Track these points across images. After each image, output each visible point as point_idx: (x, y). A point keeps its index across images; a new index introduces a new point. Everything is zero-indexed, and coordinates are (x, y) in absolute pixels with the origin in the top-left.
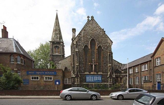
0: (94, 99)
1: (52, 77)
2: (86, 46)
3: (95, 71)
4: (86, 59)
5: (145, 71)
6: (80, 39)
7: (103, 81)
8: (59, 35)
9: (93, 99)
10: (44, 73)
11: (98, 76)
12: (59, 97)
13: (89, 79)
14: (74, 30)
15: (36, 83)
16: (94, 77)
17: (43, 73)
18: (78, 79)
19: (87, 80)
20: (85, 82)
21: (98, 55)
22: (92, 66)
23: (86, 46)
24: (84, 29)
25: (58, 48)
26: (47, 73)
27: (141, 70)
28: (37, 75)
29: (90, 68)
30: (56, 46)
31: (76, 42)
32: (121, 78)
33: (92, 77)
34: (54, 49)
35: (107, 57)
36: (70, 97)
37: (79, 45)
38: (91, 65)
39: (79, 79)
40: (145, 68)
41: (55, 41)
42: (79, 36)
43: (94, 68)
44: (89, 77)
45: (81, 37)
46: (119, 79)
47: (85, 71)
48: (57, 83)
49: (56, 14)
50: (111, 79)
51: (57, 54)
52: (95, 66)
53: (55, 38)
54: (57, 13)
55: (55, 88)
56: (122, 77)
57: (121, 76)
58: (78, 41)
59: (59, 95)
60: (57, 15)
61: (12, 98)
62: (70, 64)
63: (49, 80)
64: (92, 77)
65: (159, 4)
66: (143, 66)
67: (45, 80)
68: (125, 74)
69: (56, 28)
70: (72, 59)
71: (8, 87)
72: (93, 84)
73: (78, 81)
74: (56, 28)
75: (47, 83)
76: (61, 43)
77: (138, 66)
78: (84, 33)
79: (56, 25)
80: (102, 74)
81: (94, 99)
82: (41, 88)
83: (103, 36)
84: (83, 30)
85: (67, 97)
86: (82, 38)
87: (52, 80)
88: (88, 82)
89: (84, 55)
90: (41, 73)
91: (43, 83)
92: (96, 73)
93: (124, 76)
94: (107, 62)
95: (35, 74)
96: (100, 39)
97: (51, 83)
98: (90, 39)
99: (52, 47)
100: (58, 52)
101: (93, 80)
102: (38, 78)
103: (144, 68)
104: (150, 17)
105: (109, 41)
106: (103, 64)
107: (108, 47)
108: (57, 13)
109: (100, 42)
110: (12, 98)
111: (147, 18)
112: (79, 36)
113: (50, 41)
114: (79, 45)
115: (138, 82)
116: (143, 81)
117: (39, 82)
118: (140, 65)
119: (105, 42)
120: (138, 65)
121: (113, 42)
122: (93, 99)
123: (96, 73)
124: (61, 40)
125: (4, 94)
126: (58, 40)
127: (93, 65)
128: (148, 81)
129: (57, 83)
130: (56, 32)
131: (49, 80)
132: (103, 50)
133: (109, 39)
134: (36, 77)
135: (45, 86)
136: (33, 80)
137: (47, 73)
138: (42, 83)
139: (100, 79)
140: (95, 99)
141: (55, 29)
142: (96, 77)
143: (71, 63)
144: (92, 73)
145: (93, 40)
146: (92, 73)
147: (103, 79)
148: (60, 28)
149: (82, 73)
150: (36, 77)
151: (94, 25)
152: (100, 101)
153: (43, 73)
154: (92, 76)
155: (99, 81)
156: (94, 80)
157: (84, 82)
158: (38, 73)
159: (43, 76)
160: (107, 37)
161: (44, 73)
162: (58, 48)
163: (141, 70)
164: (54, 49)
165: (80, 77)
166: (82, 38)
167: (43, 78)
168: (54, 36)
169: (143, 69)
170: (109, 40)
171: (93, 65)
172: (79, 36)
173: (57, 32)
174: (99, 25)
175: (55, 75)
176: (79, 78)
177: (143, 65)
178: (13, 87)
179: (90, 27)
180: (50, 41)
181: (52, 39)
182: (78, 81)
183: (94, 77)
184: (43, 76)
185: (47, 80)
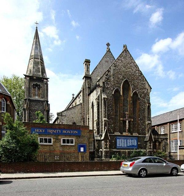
0: (143, 175)
1: (73, 140)
2: (117, 91)
3: (129, 131)
4: (116, 112)
5: (175, 132)
6: (108, 79)
7: (139, 147)
8: (41, 65)
9: (174, 174)
10: (62, 132)
11: (133, 139)
12: (120, 172)
13: (121, 143)
14: (87, 62)
15: (46, 149)
16: (127, 141)
17: (59, 131)
18: (106, 143)
19: (118, 145)
20: (115, 148)
21: (132, 106)
22: (124, 122)
23: (117, 91)
24: (115, 63)
25: (39, 89)
26: (65, 132)
27: (170, 131)
28: (49, 134)
29: (122, 125)
30: (37, 85)
31: (104, 83)
32: (160, 143)
33: (125, 140)
34: (32, 90)
35: (144, 110)
36: (174, 170)
37: (108, 87)
38: (123, 121)
39: (108, 143)
40: (176, 128)
41: (34, 75)
42: (107, 74)
43: (127, 126)
44: (120, 140)
45: (110, 76)
46: (157, 144)
47: (115, 131)
48: (82, 149)
49: (36, 28)
50: (150, 143)
51: (37, 98)
52: (129, 122)
53: (34, 71)
54: (37, 27)
55: (78, 158)
56: (161, 141)
57: (159, 140)
58: (105, 81)
59: (118, 169)
60: (37, 30)
61: (42, 178)
62: (80, 118)
63: (45, 144)
64: (125, 140)
65: (157, 39)
66: (173, 125)
67: (62, 144)
68: (164, 137)
69: (35, 52)
70: (84, 109)
71: (21, 157)
72: (127, 151)
73: (106, 146)
74: (36, 54)
75: (66, 150)
76: (45, 80)
77: (165, 125)
78: (114, 69)
79: (36, 48)
80: (138, 135)
81: (143, 175)
82: (57, 158)
83: (140, 78)
84: (113, 65)
85: (144, 171)
86: (112, 78)
87: (74, 144)
88: (120, 148)
89: (114, 104)
90: (57, 131)
91: (58, 149)
92: (130, 135)
93: (164, 139)
94: (144, 117)
95: (46, 134)
96: (136, 82)
97: (72, 150)
98: (123, 80)
99: (29, 85)
100: (39, 95)
101: (125, 146)
102: (50, 142)
103: (175, 128)
104: (147, 54)
105: (147, 86)
106: (139, 120)
107: (145, 95)
108: (37, 27)
109: (135, 87)
110: (42, 178)
111: (141, 55)
112: (107, 73)
113: (25, 75)
114: (108, 87)
115: (174, 148)
116: (179, 146)
117: (52, 147)
118: (168, 124)
119: (142, 87)
120: (166, 123)
121: (151, 88)
122: (143, 176)
123: (130, 135)
124: (45, 75)
125: (13, 171)
126: (39, 74)
127: (127, 121)
128: (182, 147)
129: (82, 149)
130: (36, 60)
131: (45, 144)
132: (139, 98)
133: (147, 83)
134: (70, 139)
135: (62, 154)
136: (42, 143)
137: (65, 132)
138: (57, 149)
139: (136, 144)
140: (145, 174)
141: (33, 54)
142: (131, 140)
143: (83, 116)
144: (124, 134)
145: (126, 83)
146: (124, 134)
147: (139, 143)
148: (42, 55)
149: (112, 133)
150: (48, 138)
151: (128, 60)
152: (179, 177)
153: (59, 131)
154: (132, 139)
155: (133, 146)
156: (127, 145)
157: (113, 149)
158: (51, 131)
159: (59, 137)
160: (144, 79)
161: (62, 132)
162: (39, 89)
163: (170, 131)
164: (32, 90)
165: (109, 140)
166: (112, 78)
167: (60, 140)
168: (31, 66)
169: (174, 129)
170: (147, 85)
171: (127, 121)
172: (107, 73)
173: (38, 60)
174: (134, 61)
175: (78, 136)
176: (108, 141)
177: (174, 125)
178: (24, 158)
179: (123, 61)
180: (25, 75)
181: (29, 72)
182: (106, 146)
183: (127, 141)
184: (59, 137)
185: (65, 144)
